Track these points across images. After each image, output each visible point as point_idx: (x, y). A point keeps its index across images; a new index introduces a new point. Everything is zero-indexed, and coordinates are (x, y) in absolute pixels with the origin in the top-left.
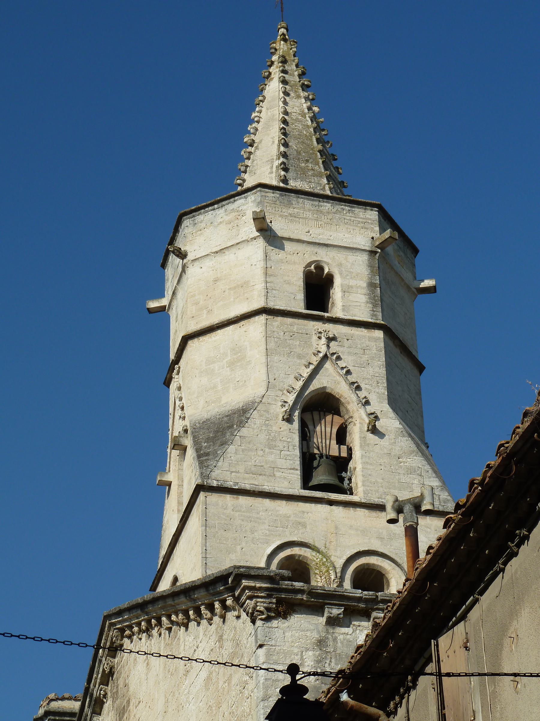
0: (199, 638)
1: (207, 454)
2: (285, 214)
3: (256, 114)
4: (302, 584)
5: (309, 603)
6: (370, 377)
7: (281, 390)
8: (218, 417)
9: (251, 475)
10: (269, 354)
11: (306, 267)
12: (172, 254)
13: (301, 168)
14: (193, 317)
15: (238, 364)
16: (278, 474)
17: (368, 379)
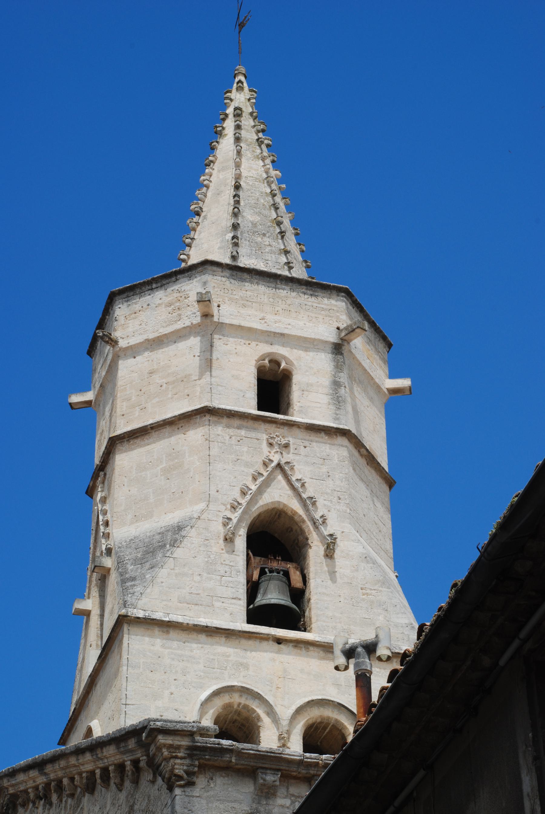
0: (106, 807)
1: (133, 579)
2: (236, 297)
3: (207, 177)
4: (230, 742)
5: (239, 767)
6: (329, 491)
7: (224, 505)
8: (148, 534)
9: (185, 605)
10: (211, 461)
11: (257, 361)
12: (100, 340)
13: (256, 243)
14: (123, 415)
15: (174, 472)
16: (217, 604)
17: (327, 494)
